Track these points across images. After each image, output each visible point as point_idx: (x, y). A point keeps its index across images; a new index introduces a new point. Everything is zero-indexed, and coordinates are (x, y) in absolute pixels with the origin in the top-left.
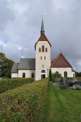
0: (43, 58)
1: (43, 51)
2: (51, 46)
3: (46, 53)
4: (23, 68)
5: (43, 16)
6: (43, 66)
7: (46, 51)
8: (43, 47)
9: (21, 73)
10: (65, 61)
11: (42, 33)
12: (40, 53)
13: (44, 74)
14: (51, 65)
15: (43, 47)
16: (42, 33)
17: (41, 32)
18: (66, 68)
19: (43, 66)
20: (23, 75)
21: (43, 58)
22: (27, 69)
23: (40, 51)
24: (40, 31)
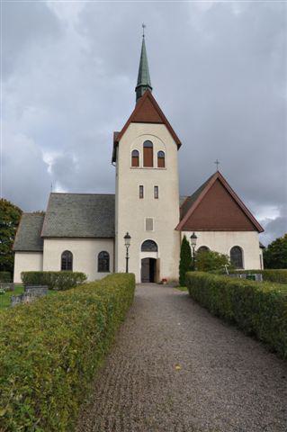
0: (149, 192)
1: (148, 163)
2: (179, 145)
3: (161, 172)
5: (144, 26)
6: (149, 225)
8: (148, 147)
11: (143, 93)
12: (135, 171)
13: (152, 255)
14: (181, 219)
15: (148, 147)
17: (138, 89)
19: (149, 225)
20: (63, 259)
21: (149, 192)
24: (135, 85)
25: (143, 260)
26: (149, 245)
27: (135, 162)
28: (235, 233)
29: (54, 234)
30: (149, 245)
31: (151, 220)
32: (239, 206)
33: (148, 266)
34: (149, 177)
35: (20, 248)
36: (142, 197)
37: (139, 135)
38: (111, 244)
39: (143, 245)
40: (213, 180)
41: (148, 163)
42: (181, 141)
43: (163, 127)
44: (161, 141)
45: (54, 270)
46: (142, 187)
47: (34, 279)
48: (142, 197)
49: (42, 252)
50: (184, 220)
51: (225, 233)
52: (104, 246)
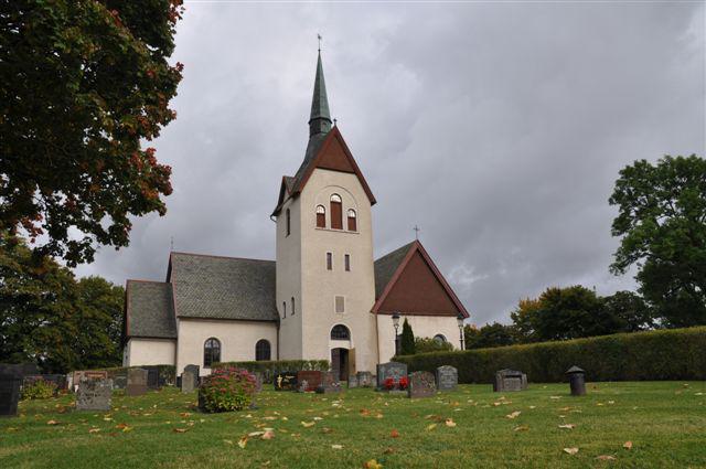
0: (338, 263)
1: (337, 224)
3: (352, 237)
4: (210, 313)
5: (319, 38)
6: (340, 304)
7: (350, 229)
8: (336, 207)
9: (193, 339)
10: (281, 348)
12: (321, 233)
13: (343, 344)
14: (377, 299)
15: (336, 207)
16: (319, 120)
17: (544, 370)
18: (441, 320)
19: (340, 304)
20: (206, 349)
21: (338, 263)
22: (229, 315)
23: (324, 226)
25: (333, 350)
26: (340, 332)
27: (321, 219)
28: (438, 318)
29: (194, 313)
30: (340, 332)
31: (342, 299)
32: (438, 279)
33: (338, 359)
34: (338, 242)
35: (140, 332)
36: (330, 267)
37: (324, 187)
38: (274, 330)
39: (333, 331)
40: (413, 251)
41: (337, 224)
42: (376, 197)
43: (353, 177)
44: (353, 201)
45: (357, 364)
46: (329, 254)
47: (158, 376)
48: (330, 267)
49: (175, 340)
50: (379, 303)
51: (427, 318)
52: (265, 333)
